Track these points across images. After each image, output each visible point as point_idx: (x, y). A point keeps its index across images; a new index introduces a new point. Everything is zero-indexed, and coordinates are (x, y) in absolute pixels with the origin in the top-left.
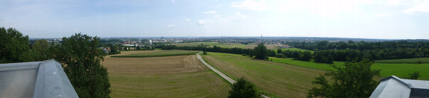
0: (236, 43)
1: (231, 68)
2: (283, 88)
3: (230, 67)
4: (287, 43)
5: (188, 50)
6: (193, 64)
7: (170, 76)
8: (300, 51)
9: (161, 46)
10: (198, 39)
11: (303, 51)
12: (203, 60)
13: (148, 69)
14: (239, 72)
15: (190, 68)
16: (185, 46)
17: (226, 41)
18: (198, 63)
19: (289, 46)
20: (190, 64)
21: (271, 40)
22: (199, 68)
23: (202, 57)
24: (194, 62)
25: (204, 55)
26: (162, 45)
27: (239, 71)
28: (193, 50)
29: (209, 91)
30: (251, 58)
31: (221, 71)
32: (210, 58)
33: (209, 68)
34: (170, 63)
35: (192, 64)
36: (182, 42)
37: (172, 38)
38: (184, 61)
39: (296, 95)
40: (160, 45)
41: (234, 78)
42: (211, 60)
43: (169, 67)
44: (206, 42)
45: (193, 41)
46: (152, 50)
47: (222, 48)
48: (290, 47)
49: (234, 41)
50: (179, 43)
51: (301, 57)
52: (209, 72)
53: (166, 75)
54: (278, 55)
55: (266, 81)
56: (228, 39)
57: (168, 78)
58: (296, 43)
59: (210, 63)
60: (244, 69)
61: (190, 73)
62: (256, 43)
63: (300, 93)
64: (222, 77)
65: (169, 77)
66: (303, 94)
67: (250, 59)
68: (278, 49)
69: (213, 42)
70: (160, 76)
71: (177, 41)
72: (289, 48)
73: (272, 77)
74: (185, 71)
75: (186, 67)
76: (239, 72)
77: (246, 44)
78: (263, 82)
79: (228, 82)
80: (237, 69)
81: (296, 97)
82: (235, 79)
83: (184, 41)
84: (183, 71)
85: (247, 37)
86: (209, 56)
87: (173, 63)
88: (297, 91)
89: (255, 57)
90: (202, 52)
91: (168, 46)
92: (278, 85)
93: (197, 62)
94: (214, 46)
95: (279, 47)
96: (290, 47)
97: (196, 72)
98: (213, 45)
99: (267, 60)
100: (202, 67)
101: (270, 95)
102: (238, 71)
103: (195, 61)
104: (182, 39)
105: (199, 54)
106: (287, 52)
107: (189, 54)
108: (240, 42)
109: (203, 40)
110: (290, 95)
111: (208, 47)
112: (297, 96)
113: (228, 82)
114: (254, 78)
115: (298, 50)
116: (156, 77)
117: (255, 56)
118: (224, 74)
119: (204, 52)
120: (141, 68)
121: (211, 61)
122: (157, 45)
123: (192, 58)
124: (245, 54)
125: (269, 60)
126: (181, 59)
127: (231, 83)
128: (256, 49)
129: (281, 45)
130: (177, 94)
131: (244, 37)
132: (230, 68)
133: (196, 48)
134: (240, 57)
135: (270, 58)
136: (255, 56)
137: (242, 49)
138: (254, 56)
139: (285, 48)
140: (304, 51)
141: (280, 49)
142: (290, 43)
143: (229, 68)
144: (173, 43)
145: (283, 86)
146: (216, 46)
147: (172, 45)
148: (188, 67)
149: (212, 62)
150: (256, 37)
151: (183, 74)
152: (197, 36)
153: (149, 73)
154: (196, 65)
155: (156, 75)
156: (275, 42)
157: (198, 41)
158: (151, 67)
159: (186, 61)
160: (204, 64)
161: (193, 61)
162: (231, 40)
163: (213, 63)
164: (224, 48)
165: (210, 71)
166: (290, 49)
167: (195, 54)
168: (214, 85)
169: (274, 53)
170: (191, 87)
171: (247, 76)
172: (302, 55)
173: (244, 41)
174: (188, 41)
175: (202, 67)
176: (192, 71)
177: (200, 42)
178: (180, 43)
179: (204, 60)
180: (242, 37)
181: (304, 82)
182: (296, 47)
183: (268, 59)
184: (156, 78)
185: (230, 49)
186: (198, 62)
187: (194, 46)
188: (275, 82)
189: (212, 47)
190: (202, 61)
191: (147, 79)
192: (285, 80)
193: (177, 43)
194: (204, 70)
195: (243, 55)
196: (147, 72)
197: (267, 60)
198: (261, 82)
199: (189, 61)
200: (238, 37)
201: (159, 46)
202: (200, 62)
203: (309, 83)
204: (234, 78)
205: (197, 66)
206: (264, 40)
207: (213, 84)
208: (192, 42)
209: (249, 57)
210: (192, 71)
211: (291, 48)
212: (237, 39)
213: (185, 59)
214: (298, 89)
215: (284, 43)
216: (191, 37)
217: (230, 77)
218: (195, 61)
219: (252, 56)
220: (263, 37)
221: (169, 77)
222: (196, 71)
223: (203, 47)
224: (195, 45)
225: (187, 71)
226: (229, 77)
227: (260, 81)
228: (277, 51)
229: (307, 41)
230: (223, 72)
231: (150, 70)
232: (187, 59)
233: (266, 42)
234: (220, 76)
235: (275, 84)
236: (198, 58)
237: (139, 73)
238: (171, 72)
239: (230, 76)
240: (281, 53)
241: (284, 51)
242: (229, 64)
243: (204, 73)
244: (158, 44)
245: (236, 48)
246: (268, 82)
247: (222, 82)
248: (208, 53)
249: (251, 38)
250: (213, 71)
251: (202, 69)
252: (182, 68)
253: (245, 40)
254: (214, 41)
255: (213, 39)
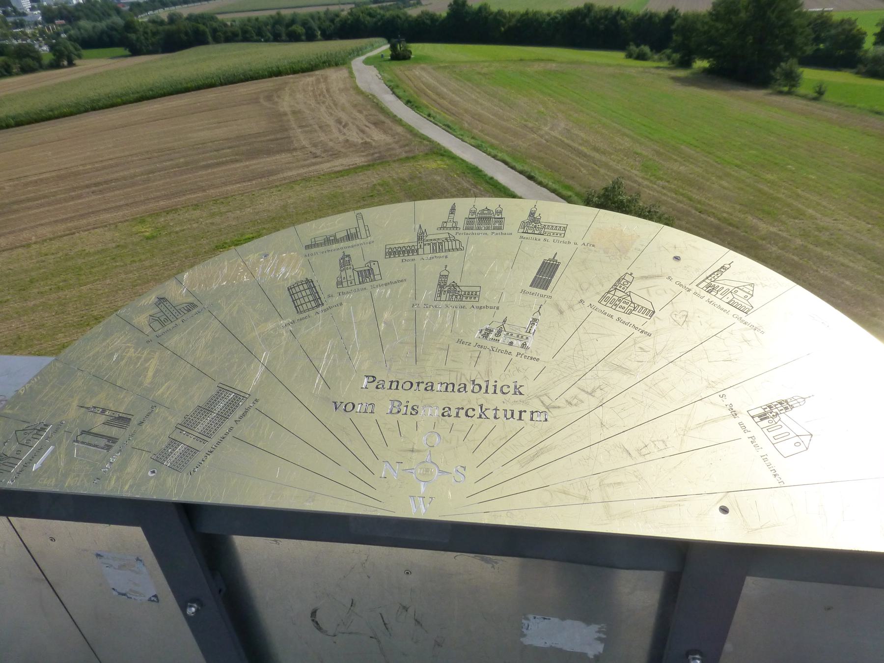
1: (554, 133)
3: (546, 129)
5: (294, 37)
6: (339, 121)
7: (223, 209)
9: (112, 28)
12: (394, 93)
13: (80, 197)
14: (597, 156)
15: (325, 151)
16: (272, 17)
20: (323, 127)
23: (383, 78)
24: (343, 110)
25: (398, 67)
26: (118, 20)
27: (596, 149)
28: (327, 36)
30: (681, 73)
31: (494, 152)
35: (331, 122)
38: (285, 114)
40: (102, 25)
41: (569, 188)
42: (438, 94)
46: (55, 65)
47: (500, 13)
52: (433, 164)
53: (196, 206)
55: (750, 218)
57: (212, 224)
61: (329, 174)
67: (676, 79)
70: (169, 217)
73: (790, 201)
74: (302, 171)
75: (304, 147)
78: (730, 224)
82: (569, 193)
84: (290, 169)
86: (423, 69)
90: (383, 48)
91: (162, 23)
93: (360, 112)
97: (362, 167)
99: (786, 89)
100: (389, 139)
105: (367, 62)
107: (305, 65)
114: (682, 194)
116: (147, 230)
118: (513, 168)
119: (393, 48)
120: (28, 200)
121: (434, 97)
122: (83, 23)
123: (328, 91)
124: (646, 49)
125: (802, 90)
126: (266, 104)
132: (547, 133)
133: (344, 23)
137: (632, 14)
138: (701, 64)
145: (851, 264)
147: (190, 18)
149: (445, 103)
151: (292, 188)
153: (92, 219)
154: (357, 126)
155: (142, 221)
158: (93, 181)
159: (294, 113)
161: (336, 105)
164: (512, 15)
165: (437, 154)
169: (854, 39)
171: (640, 180)
175: (389, 139)
179: (401, 94)
183: (793, 86)
184: (148, 238)
188: (805, 235)
191: (98, 252)
194: (404, 155)
195: (629, 56)
196: (82, 216)
197: (789, 93)
198: (719, 219)
199: (313, 110)
201: (103, 32)
202: (374, 111)
204: (569, 188)
205: (363, 132)
209: (665, 64)
210: (339, 164)
217: (545, 186)
219: (685, 63)
222: (359, 160)
225: (309, 166)
226: (540, 184)
228: (878, 30)
230: (508, 159)
231: (94, 197)
232: (300, 96)
234: (492, 178)
235: (799, 241)
236: (359, 84)
237: (25, 235)
238: (224, 189)
239: (545, 181)
244: (88, 17)
248: (417, 49)
250: (453, 157)
251: (393, 149)
252: (280, 152)
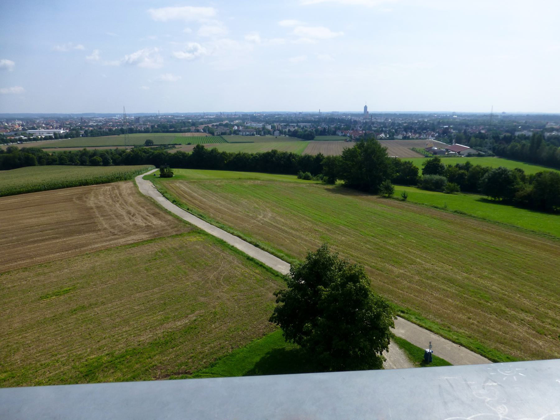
0: (273, 134)
2: (448, 297)
4: (464, 137)
5: (94, 163)
6: (129, 213)
7: (46, 271)
8: (520, 171)
10: (131, 123)
11: (530, 170)
12: (164, 196)
14: (294, 232)
15: (121, 231)
17: (236, 128)
18: (147, 210)
19: (471, 147)
20: (119, 216)
21: (399, 124)
22: (155, 225)
24: (131, 205)
25: (165, 181)
27: (292, 228)
28: (116, 163)
29: (202, 299)
30: (330, 187)
31: (232, 231)
32: (189, 188)
33: (190, 224)
34: (33, 221)
35: (124, 213)
36: (66, 136)
37: (14, 119)
38: (92, 208)
39: (499, 327)
42: (192, 197)
43: (31, 237)
44: (164, 132)
45: (110, 130)
47: (224, 153)
48: (473, 151)
49: (264, 128)
50: (50, 138)
51: (521, 193)
52: (193, 239)
54: (426, 181)
56: (241, 121)
58: (502, 136)
59: (190, 208)
60: (309, 225)
61: (124, 245)
62: (344, 136)
63: (513, 325)
64: (241, 252)
65: (45, 274)
66: (525, 328)
67: (328, 190)
68: (429, 159)
69: (188, 135)
71: (43, 132)
72: (469, 155)
74: (104, 244)
75: (105, 229)
76: (294, 232)
77: (307, 136)
78: (377, 269)
79: (261, 265)
80: (286, 224)
81: (497, 334)
82: (282, 254)
83: (74, 132)
84: (96, 243)
85: (312, 115)
86: (181, 183)
87: (42, 219)
88: (500, 313)
89: (342, 185)
90: (154, 171)
92: (429, 282)
93: (143, 207)
94: (195, 146)
95: (429, 149)
96: (473, 151)
98: (189, 144)
99: (387, 195)
100: (163, 224)
101: (403, 312)
102: (291, 231)
103: (134, 203)
104: (61, 121)
105: (145, 178)
106: (462, 171)
108: (287, 130)
109: (153, 127)
110: (473, 324)
111: (172, 151)
112: (500, 330)
113: (261, 265)
115: (510, 165)
117: (342, 182)
118: (245, 240)
119: (162, 170)
123: (120, 194)
125: (395, 196)
127: (271, 268)
128: (349, 155)
129: (436, 145)
130: (91, 327)
131: (300, 113)
132: (261, 219)
133: (128, 155)
134: (290, 182)
135: (399, 189)
136: (342, 182)
138: (339, 182)
139: (454, 155)
140: (538, 172)
141: (437, 160)
142: (476, 137)
143: (259, 221)
144: (26, 140)
145: (448, 289)
146: (203, 147)
147: (23, 150)
148: (113, 228)
150: (346, 115)
151: (98, 255)
152: (127, 112)
154: (142, 216)
156: (415, 132)
157: (131, 131)
159: (98, 207)
160: (169, 213)
161: (126, 203)
162: (255, 125)
163: (199, 207)
164: (231, 155)
166: (475, 162)
167: (130, 179)
168: (217, 279)
169: (414, 171)
170: (137, 295)
172: (529, 188)
173: (299, 127)
174: (92, 131)
175: (163, 224)
176: (129, 238)
177: (140, 132)
178: (56, 138)
179: (169, 197)
180: (295, 114)
181: (532, 287)
182: (501, 154)
183: (390, 194)
185: (252, 155)
186: (146, 208)
187: (120, 148)
188: (419, 273)
189: (189, 150)
190: (161, 200)
192: (456, 270)
193: (41, 139)
194: (174, 233)
195: (300, 177)
197: (389, 197)
200: (278, 115)
202: (152, 207)
203: (553, 296)
205: (146, 219)
206: (373, 123)
207: (211, 276)
208: (106, 134)
209: (320, 182)
210: (130, 239)
211: (479, 155)
212: (277, 122)
213: (92, 199)
214: (507, 310)
215: (450, 137)
216: (100, 115)
217: (267, 251)
218: (134, 203)
220: (373, 115)
221: (45, 274)
222: (144, 236)
223: (156, 152)
224: (122, 144)
226: (263, 249)
227: (368, 265)
228: (423, 167)
229: (552, 130)
230: (242, 235)
232: (101, 198)
233: (382, 131)
234: (233, 246)
235: (417, 278)
236: (141, 191)
239: (266, 248)
240: (440, 174)
241: (450, 166)
242: (255, 207)
243: (175, 243)
245: (274, 152)
246: (395, 269)
247: (240, 265)
248: (176, 172)
249: (326, 118)
250: (207, 234)
251: (166, 230)
252: (88, 232)
253: (302, 125)
254: (193, 128)
255: (189, 122)
